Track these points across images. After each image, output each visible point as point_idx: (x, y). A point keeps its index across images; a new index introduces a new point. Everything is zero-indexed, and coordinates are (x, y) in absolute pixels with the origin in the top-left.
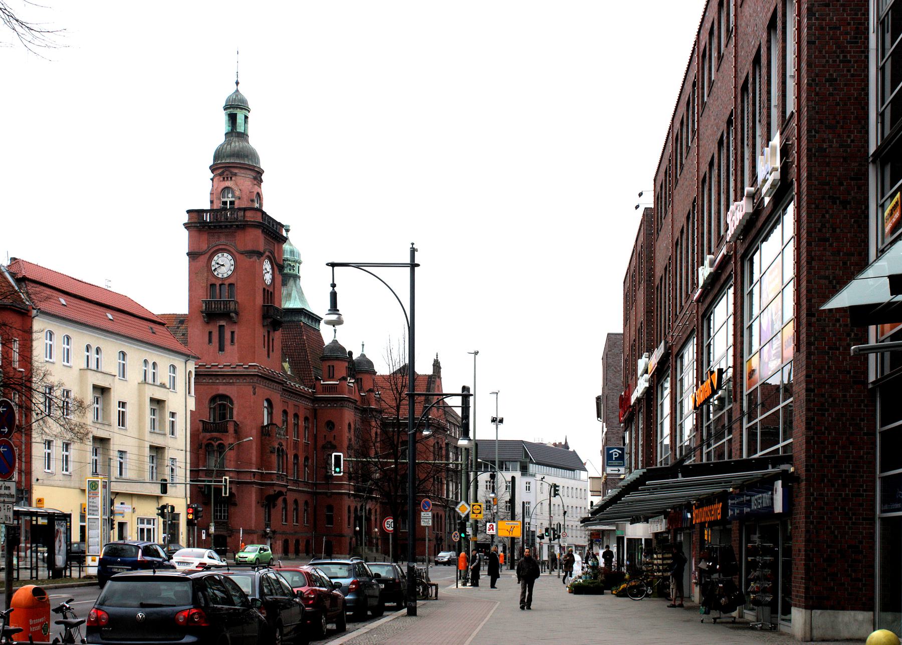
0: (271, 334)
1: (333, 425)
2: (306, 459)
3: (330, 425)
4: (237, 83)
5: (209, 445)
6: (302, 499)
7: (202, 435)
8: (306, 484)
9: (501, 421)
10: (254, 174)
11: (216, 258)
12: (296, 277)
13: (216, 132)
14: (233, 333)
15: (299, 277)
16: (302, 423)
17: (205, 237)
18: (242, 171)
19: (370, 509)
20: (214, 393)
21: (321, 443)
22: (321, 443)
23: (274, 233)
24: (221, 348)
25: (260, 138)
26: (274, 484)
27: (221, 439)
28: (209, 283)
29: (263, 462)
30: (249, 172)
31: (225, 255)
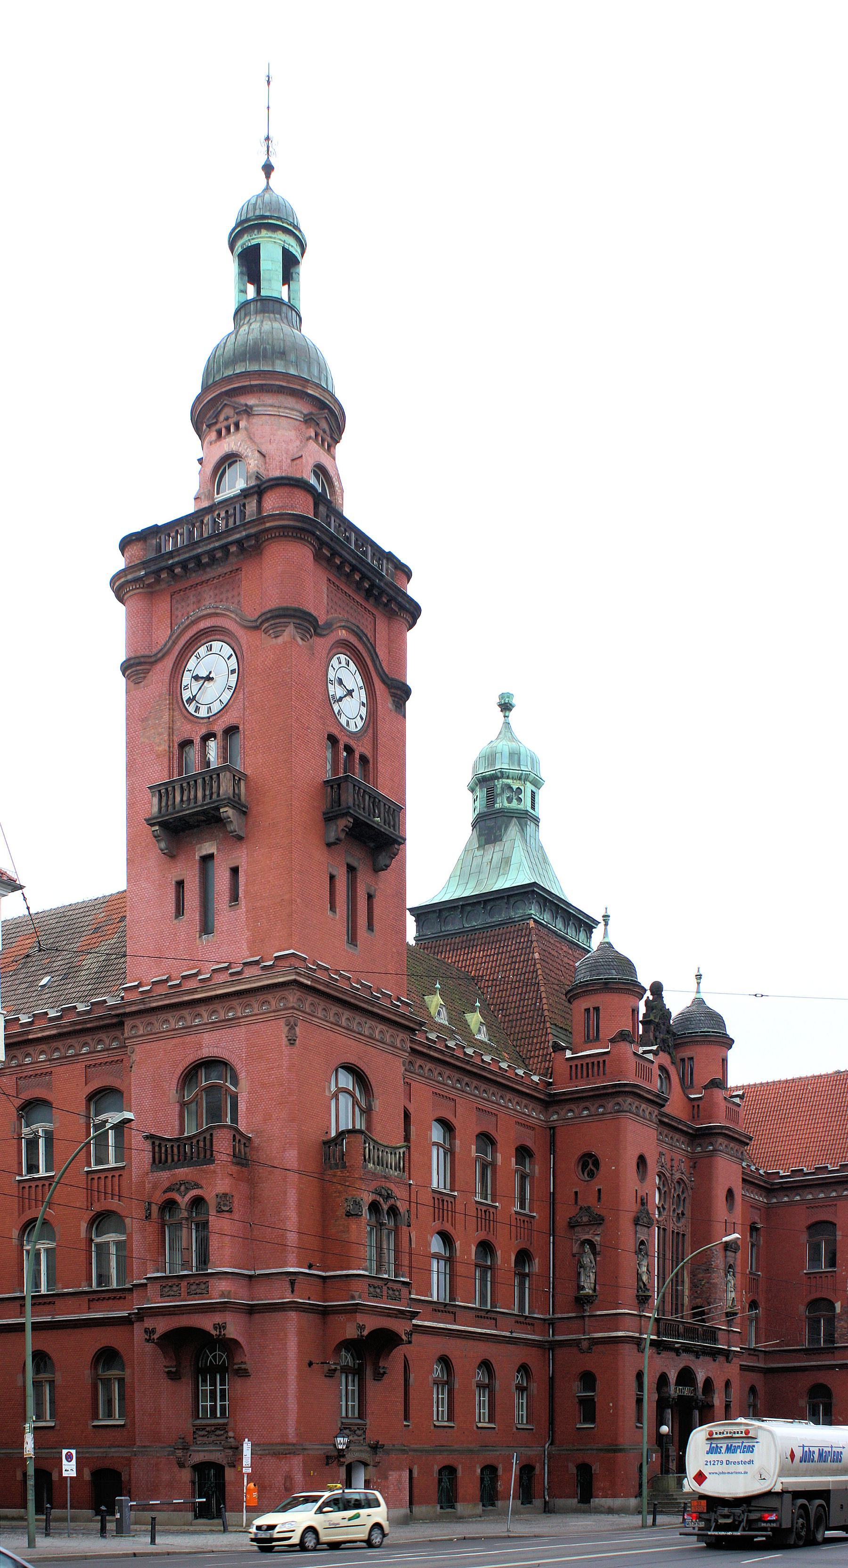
1: (596, 1163)
2: (523, 1256)
3: (589, 1163)
4: (268, 169)
5: (170, 1205)
6: (506, 1361)
7: (152, 1177)
8: (523, 1321)
10: (306, 408)
11: (192, 663)
12: (527, 818)
13: (206, 313)
14: (235, 871)
15: (536, 820)
16: (505, 1159)
17: (163, 606)
18: (269, 399)
19: (708, 1382)
20: (191, 1057)
21: (564, 1214)
22: (564, 1214)
23: (373, 592)
24: (206, 928)
25: (331, 322)
26: (355, 1309)
27: (197, 1186)
28: (177, 740)
29: (327, 1244)
30: (290, 402)
31: (216, 645)
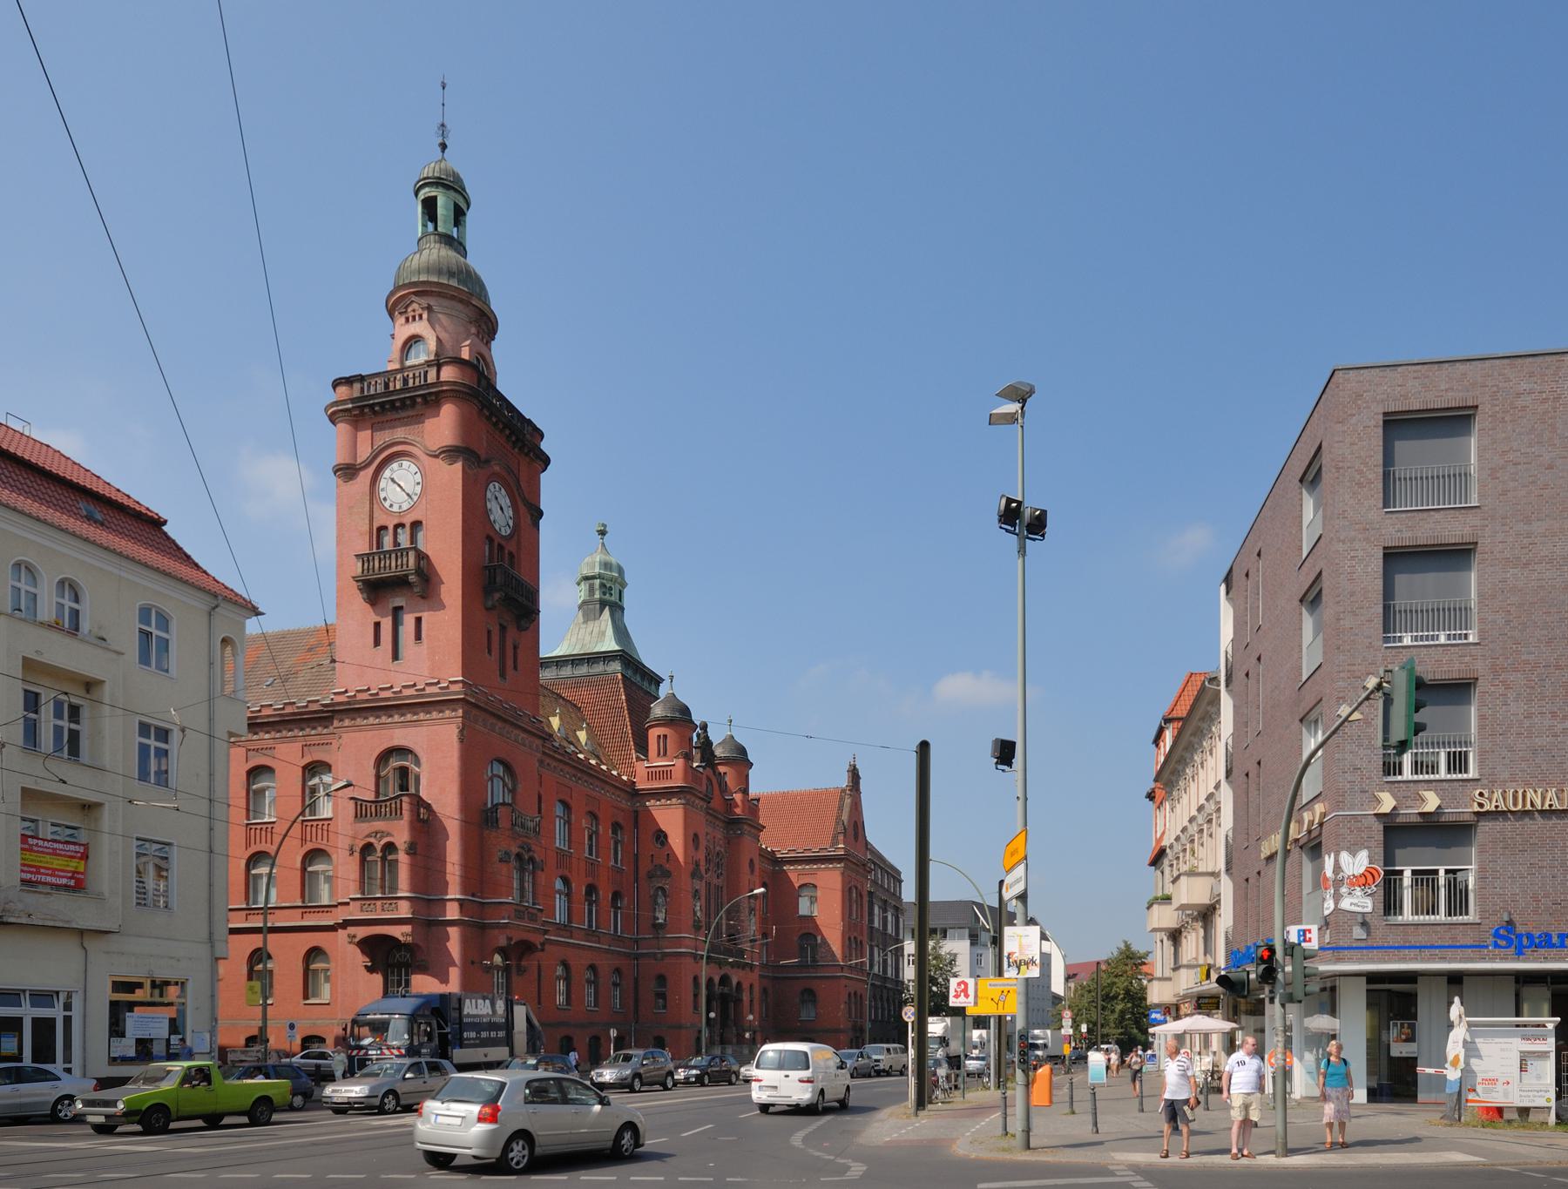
0: (512, 631)
2: (616, 896)
9: (1038, 525)
14: (419, 620)
16: (605, 830)
21: (645, 866)
27: (389, 834)
